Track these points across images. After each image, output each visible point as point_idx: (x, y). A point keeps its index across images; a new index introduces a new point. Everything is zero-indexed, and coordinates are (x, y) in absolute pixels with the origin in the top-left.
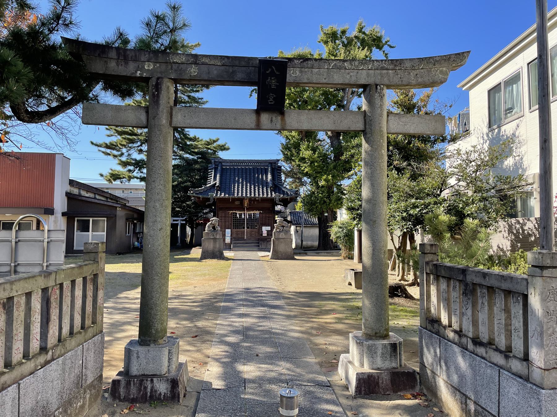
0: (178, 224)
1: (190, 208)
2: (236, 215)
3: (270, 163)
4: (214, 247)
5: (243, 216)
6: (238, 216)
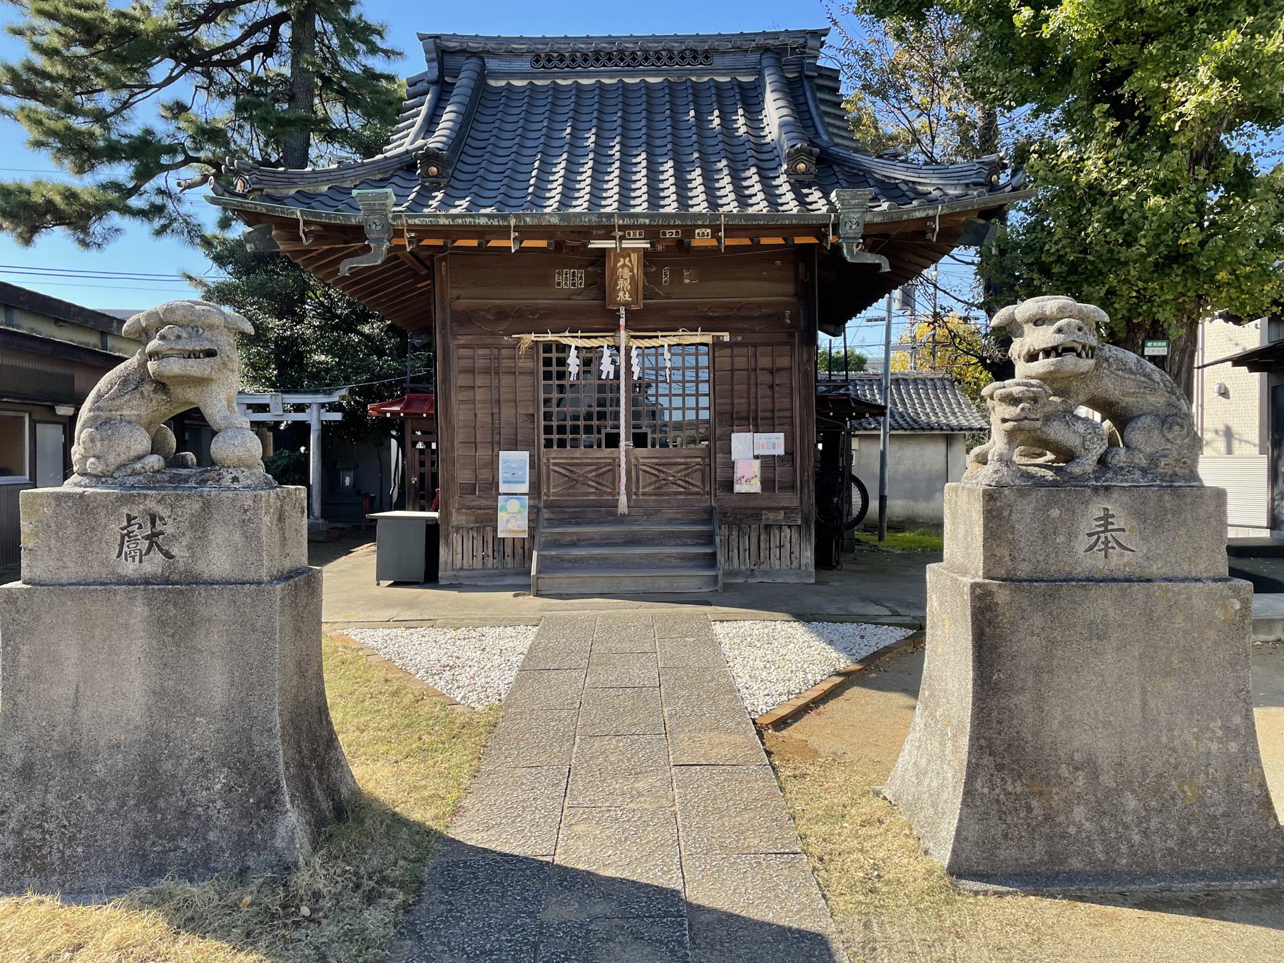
1: (381, 353)
2: (562, 362)
3: (766, 50)
4: (168, 701)
5: (607, 367)
6: (573, 363)
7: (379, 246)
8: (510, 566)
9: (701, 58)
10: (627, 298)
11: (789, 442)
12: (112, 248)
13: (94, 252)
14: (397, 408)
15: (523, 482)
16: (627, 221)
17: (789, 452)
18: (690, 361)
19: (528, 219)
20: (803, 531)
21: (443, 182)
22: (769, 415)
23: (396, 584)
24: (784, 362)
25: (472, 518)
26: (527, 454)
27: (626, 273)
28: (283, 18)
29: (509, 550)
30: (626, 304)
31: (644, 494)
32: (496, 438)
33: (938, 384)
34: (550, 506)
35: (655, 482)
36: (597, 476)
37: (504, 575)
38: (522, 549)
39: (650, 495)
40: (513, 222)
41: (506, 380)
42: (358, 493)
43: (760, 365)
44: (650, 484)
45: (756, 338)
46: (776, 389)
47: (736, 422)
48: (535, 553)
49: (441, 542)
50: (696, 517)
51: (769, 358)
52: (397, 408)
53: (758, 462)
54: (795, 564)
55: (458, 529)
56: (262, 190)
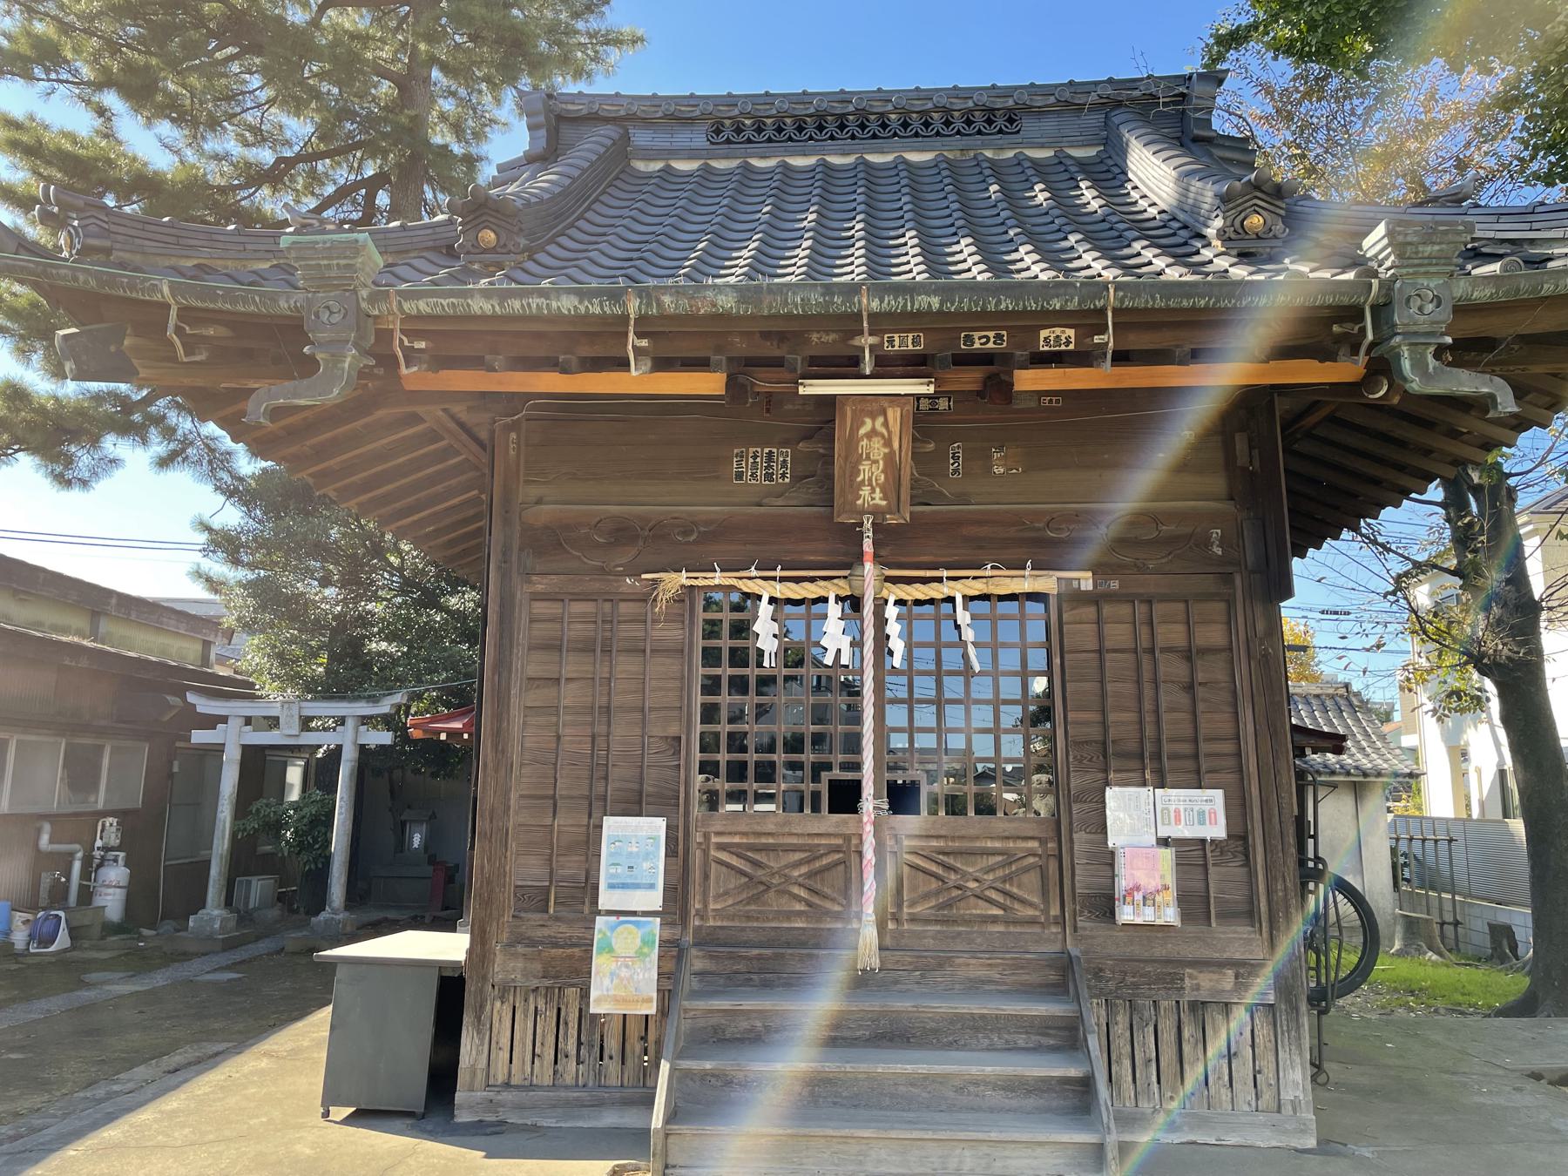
0: (219, 749)
2: (742, 629)
6: (765, 630)
7: (337, 358)
8: (613, 1080)
9: (1000, 122)
10: (879, 500)
11: (1237, 808)
12: (102, 486)
13: (75, 494)
14: (458, 725)
15: (652, 886)
16: (890, 303)
17: (1239, 835)
18: (1008, 632)
19: (667, 299)
20: (1282, 1019)
21: (509, 260)
22: (1186, 748)
23: (364, 1116)
24: (1212, 635)
25: (537, 967)
26: (658, 825)
27: (877, 449)
28: (379, 181)
29: (612, 1045)
30: (876, 512)
31: (913, 919)
32: (599, 788)
33: (1328, 703)
34: (706, 940)
35: (938, 893)
36: (811, 875)
37: (599, 1104)
38: (641, 1039)
39: (927, 921)
40: (633, 306)
41: (626, 666)
42: (432, 860)
43: (1161, 641)
44: (926, 896)
45: (1150, 584)
46: (1201, 692)
47: (1113, 763)
48: (665, 1067)
49: (467, 1019)
50: (1034, 978)
51: (1181, 628)
52: (458, 725)
53: (1168, 854)
54: (1267, 1097)
55: (505, 991)
56: (108, 251)
